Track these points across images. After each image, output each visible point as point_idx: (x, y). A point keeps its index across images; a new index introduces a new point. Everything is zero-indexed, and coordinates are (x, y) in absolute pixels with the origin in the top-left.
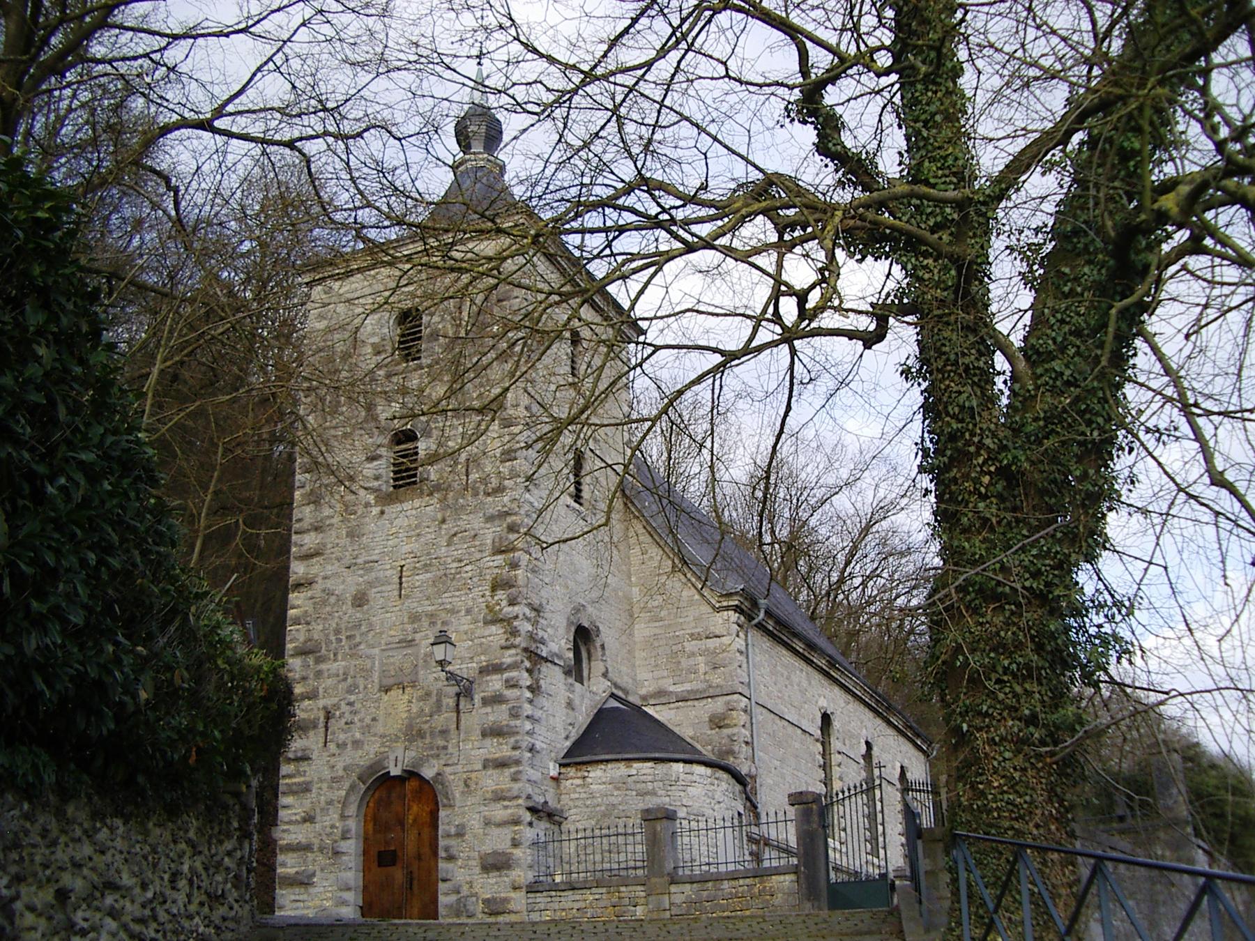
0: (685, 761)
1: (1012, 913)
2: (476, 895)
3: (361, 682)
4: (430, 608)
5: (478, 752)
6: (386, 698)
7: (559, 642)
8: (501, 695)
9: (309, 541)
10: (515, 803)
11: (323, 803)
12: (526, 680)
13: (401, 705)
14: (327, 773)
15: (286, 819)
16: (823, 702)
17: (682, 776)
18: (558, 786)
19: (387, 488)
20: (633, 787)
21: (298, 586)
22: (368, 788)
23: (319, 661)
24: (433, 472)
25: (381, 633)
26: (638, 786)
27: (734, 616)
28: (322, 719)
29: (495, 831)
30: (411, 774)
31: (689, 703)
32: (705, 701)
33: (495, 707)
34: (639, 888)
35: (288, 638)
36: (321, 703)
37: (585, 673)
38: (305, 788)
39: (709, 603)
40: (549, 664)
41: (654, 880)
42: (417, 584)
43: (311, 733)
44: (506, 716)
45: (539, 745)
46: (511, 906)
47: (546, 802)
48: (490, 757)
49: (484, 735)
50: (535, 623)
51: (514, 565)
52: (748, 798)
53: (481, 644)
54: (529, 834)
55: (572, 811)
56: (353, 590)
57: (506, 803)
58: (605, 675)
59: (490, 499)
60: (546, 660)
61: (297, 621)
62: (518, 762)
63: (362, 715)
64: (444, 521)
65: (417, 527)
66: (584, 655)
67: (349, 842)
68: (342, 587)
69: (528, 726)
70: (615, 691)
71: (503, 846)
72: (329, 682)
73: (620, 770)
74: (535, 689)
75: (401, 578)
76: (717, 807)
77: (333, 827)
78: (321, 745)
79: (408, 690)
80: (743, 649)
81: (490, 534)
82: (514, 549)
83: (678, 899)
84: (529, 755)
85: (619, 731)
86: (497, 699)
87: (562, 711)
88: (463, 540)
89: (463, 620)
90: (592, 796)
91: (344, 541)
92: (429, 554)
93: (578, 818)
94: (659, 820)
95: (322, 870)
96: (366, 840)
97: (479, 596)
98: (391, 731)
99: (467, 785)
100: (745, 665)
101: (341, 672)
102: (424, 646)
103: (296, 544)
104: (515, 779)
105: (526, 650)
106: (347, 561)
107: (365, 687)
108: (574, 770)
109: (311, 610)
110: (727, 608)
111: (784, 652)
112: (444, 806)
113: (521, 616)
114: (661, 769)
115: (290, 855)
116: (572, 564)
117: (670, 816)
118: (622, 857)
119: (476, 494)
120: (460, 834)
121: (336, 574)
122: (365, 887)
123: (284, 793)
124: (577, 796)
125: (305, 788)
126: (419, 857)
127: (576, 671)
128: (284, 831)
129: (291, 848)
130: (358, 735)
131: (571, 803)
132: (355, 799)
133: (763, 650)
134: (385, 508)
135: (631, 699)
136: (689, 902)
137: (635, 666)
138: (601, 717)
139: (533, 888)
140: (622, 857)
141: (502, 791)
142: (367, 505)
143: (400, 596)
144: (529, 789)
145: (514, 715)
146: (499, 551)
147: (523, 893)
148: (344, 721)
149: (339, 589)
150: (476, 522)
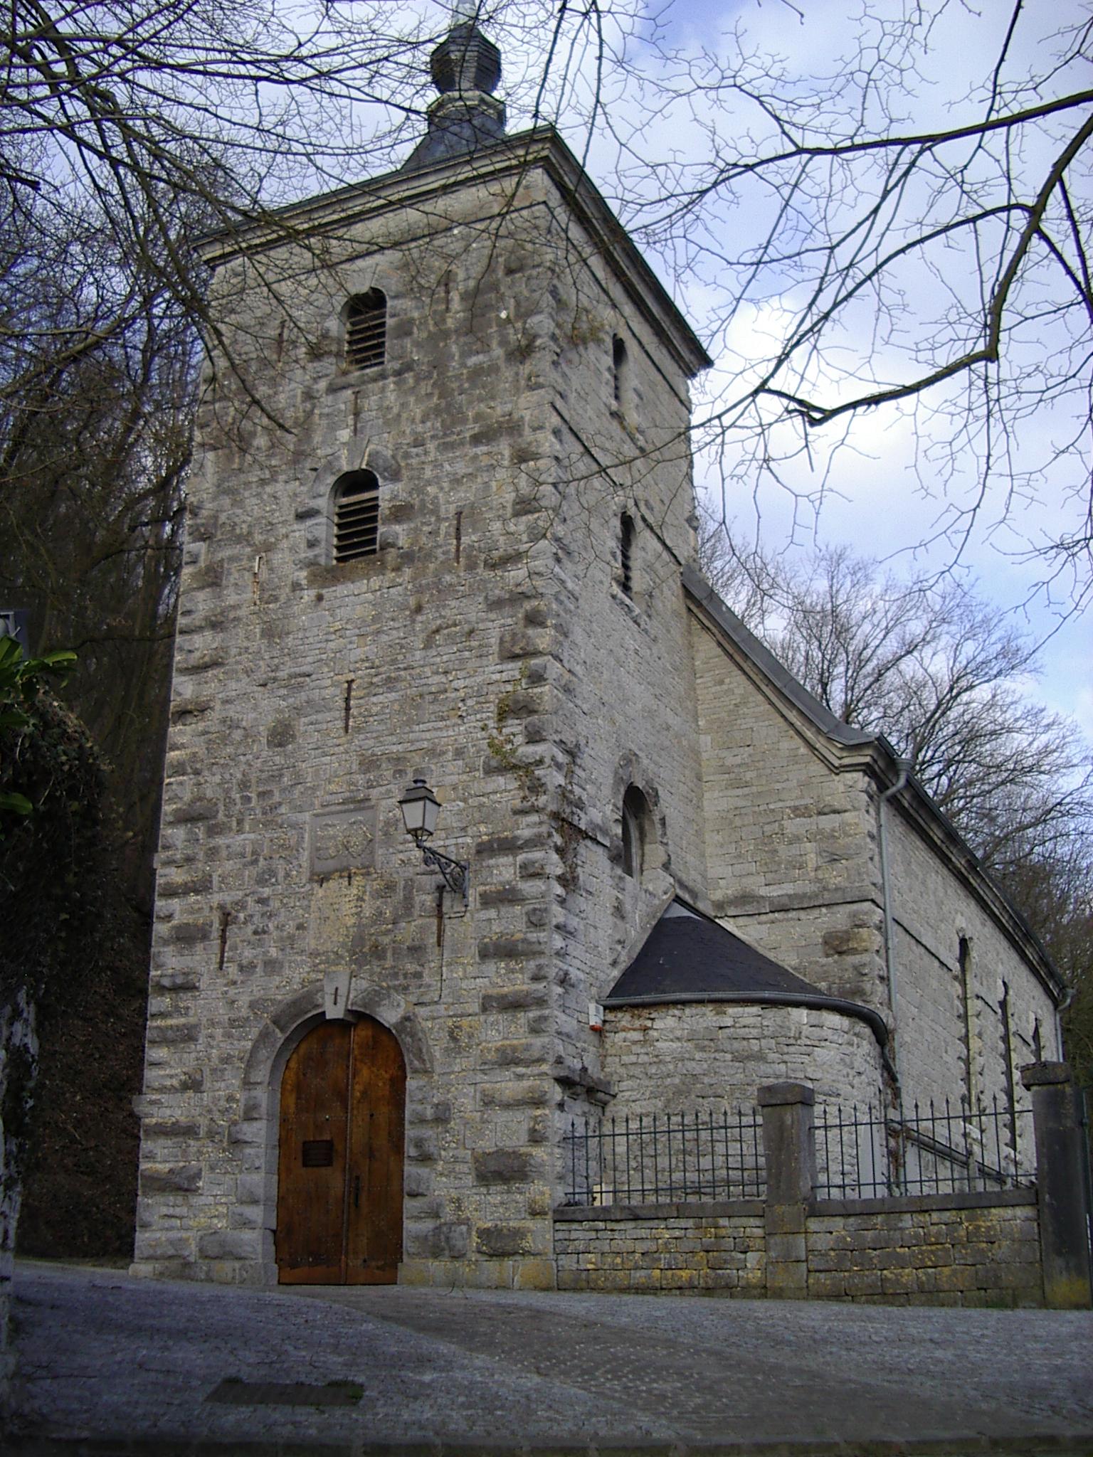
2: (467, 1222)
3: (281, 867)
4: (394, 749)
5: (470, 984)
6: (320, 892)
7: (602, 810)
8: (513, 890)
10: (535, 1070)
11: (215, 1061)
12: (555, 866)
13: (344, 906)
14: (223, 1013)
15: (156, 1085)
16: (961, 922)
17: (806, 1030)
18: (602, 1043)
19: (327, 553)
20: (727, 1046)
21: (183, 714)
22: (287, 1039)
23: (212, 831)
25: (314, 789)
26: (736, 1045)
27: (861, 780)
28: (216, 925)
29: (500, 1117)
30: (360, 1018)
31: (792, 915)
32: (816, 912)
33: (503, 910)
34: (752, 1221)
35: (165, 797)
36: (216, 899)
38: (188, 1035)
39: (824, 760)
40: (589, 843)
41: (780, 1209)
42: (375, 710)
43: (199, 947)
44: (521, 925)
45: (574, 974)
47: (584, 1069)
48: (493, 991)
49: (484, 954)
50: (570, 774)
51: (536, 678)
53: (482, 805)
54: (558, 1122)
55: (624, 1085)
56: (270, 720)
57: (521, 1070)
58: (666, 866)
60: (586, 836)
61: (180, 769)
62: (541, 1002)
63: (282, 919)
64: (419, 609)
65: (375, 619)
67: (256, 1125)
69: (558, 942)
71: (515, 1142)
72: (229, 865)
73: (705, 1018)
74: (569, 881)
75: (347, 700)
76: (856, 1081)
77: (230, 1099)
78: (214, 966)
79: (357, 880)
80: (875, 831)
81: (495, 627)
82: (536, 653)
83: (822, 1242)
84: (560, 990)
85: (684, 959)
86: (507, 897)
87: (604, 924)
88: (451, 639)
89: (450, 767)
90: (658, 1060)
91: (258, 643)
92: (394, 661)
93: (635, 1095)
94: (787, 1104)
95: (212, 1169)
96: (284, 1121)
97: (472, 732)
98: (329, 946)
99: (454, 1039)
100: (876, 858)
101: (249, 849)
103: (181, 649)
104: (535, 1030)
105: (556, 816)
106: (260, 676)
107: (287, 875)
108: (628, 1016)
111: (919, 843)
112: (415, 1071)
113: (547, 761)
114: (773, 1017)
115: (162, 1141)
116: (620, 687)
117: (805, 1099)
118: (705, 1163)
119: (471, 567)
120: (442, 1118)
122: (281, 1199)
123: (153, 1042)
124: (633, 1059)
125: (188, 1035)
126: (371, 1153)
127: (622, 858)
128: (152, 1103)
129: (163, 1131)
130: (273, 952)
131: (622, 1071)
132: (266, 1056)
134: (324, 591)
135: (701, 906)
137: (709, 857)
138: (663, 930)
139: (565, 1214)
140: (705, 1163)
141: (514, 1049)
142: (296, 586)
143: (346, 728)
144: (560, 1048)
147: (548, 1222)
148: (250, 928)
149: (248, 719)
150: (473, 611)
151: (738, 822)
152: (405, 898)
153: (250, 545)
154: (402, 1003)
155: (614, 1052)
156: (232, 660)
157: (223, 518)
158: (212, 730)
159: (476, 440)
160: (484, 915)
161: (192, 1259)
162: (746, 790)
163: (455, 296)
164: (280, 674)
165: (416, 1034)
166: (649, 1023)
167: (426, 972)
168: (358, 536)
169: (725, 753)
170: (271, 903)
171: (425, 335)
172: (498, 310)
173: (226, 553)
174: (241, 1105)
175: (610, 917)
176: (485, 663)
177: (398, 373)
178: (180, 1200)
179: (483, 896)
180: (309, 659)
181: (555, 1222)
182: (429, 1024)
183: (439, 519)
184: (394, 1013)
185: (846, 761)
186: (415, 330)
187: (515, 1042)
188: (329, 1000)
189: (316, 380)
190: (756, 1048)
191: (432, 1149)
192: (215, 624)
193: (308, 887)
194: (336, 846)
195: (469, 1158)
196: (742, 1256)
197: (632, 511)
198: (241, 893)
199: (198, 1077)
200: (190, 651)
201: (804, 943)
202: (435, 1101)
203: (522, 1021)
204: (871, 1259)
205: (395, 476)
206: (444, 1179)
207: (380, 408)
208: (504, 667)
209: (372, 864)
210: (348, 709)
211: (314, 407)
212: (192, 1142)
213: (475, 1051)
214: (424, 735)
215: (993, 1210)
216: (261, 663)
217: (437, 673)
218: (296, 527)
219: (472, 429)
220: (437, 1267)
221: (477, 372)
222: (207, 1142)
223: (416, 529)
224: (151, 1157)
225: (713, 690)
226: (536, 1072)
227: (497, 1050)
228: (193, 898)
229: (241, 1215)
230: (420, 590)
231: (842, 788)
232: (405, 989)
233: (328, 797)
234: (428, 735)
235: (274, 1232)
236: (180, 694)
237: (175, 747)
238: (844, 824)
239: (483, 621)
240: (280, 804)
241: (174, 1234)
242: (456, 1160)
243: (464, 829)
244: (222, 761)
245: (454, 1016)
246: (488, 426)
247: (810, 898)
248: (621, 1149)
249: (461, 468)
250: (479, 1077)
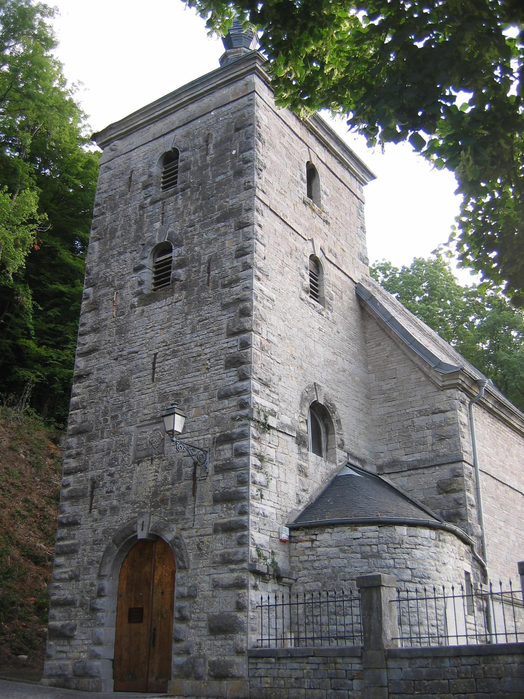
1: (113, 176)
2: (204, 657)
3: (120, 455)
4: (175, 388)
5: (209, 517)
6: (138, 469)
9: (89, 340)
13: (149, 475)
15: (58, 577)
17: (406, 539)
19: (148, 288)
21: (80, 377)
23: (89, 439)
24: (181, 273)
25: (137, 412)
28: (89, 489)
29: (222, 593)
30: (155, 538)
31: (420, 471)
36: (90, 474)
37: (324, 446)
39: (434, 383)
42: (167, 368)
44: (234, 482)
46: (235, 671)
48: (219, 521)
52: (475, 559)
53: (216, 416)
57: (233, 567)
59: (227, 290)
65: (169, 320)
67: (104, 599)
68: (111, 375)
70: (351, 461)
71: (229, 609)
72: (97, 456)
75: (154, 364)
77: (92, 585)
79: (156, 461)
81: (226, 320)
83: (396, 675)
92: (177, 341)
93: (307, 579)
96: (120, 596)
98: (141, 498)
99: (200, 549)
101: (106, 447)
106: (115, 355)
107: (123, 460)
109: (86, 396)
111: (504, 427)
112: (180, 568)
119: (215, 287)
120: (191, 596)
121: (107, 366)
124: (306, 558)
129: (58, 604)
130: (115, 503)
131: (300, 565)
135: (368, 468)
141: (229, 554)
142: (133, 306)
143: (153, 379)
146: (232, 334)
148: (105, 490)
150: (215, 310)
151: (389, 420)
152: (178, 470)
153: (112, 287)
154: (175, 530)
155: (295, 554)
156: (102, 347)
157: (101, 274)
158: (92, 384)
159: (218, 220)
160: (216, 478)
161: (70, 677)
162: (393, 403)
163: (211, 146)
164: (124, 353)
165: (181, 546)
166: (314, 537)
167: (187, 510)
168: (163, 277)
169: (382, 383)
170: (115, 476)
171: (196, 168)
172: (231, 151)
173: (103, 292)
174: (97, 587)
175: (298, 476)
176: (220, 338)
177: (183, 190)
178: (66, 643)
179: (216, 467)
180: (138, 344)
181: (249, 657)
182: (188, 541)
183: (200, 265)
184: (171, 535)
185: (446, 383)
186: (192, 167)
187: (230, 550)
188: (139, 528)
189: (145, 198)
190: (375, 551)
191: (188, 614)
192: (95, 330)
193: (132, 466)
194: (146, 443)
195: (206, 618)
196: (350, 682)
197: (319, 254)
198: (101, 471)
199: (77, 572)
200: (84, 344)
201: (427, 487)
202: (190, 585)
203: (234, 538)
204: (425, 687)
205: (180, 245)
206: (193, 631)
207: (174, 209)
208: (229, 340)
209: (163, 453)
210: (154, 368)
211: (144, 213)
212: (73, 609)
214: (190, 380)
215: (500, 658)
216: (115, 348)
217: (196, 346)
218: (134, 275)
219: (218, 214)
220: (188, 684)
221: (220, 185)
222: (80, 609)
223: (189, 270)
224: (53, 618)
225: (375, 349)
226: (240, 567)
227: (221, 555)
228: (79, 475)
229: (93, 651)
230: (189, 303)
231: (445, 399)
232: (176, 521)
233: (143, 417)
234: (191, 380)
235: (113, 660)
236: (78, 367)
237: (75, 395)
238: (446, 418)
239: (219, 316)
240: (121, 422)
241: (62, 662)
242: (199, 620)
243: (208, 430)
244: (96, 401)
245: (201, 535)
246: (225, 212)
247: (429, 461)
248: (301, 611)
249: (211, 236)
250: (212, 571)
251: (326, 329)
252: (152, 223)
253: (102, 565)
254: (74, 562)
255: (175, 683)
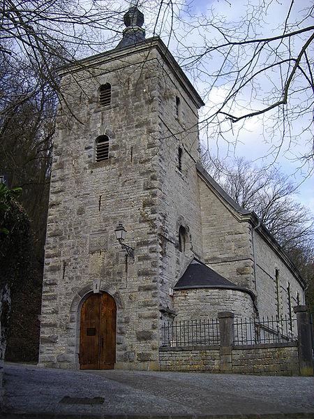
0: (233, 289)
7: (173, 233)
9: (58, 185)
13: (99, 260)
16: (276, 265)
19: (94, 159)
23: (61, 239)
24: (115, 153)
29: (144, 321)
36: (62, 259)
37: (183, 249)
38: (54, 298)
44: (150, 266)
47: (168, 307)
49: (139, 275)
54: (160, 323)
57: (149, 308)
58: (191, 249)
61: (51, 221)
62: (156, 288)
64: (120, 175)
66: (182, 240)
72: (66, 249)
73: (203, 292)
81: (142, 181)
83: (236, 357)
86: (146, 258)
89: (129, 221)
91: (74, 185)
94: (226, 318)
97: (135, 211)
102: (111, 232)
105: (160, 235)
106: (75, 194)
110: (245, 221)
114: (222, 292)
117: (232, 316)
118: (203, 334)
119: (135, 163)
120: (127, 322)
122: (81, 345)
125: (54, 298)
133: (257, 239)
136: (242, 359)
137: (204, 247)
140: (203, 334)
141: (148, 302)
142: (85, 169)
145: (154, 265)
147: (157, 352)
150: (136, 176)
159: (137, 126)
163: (131, 85)
168: (103, 154)
197: (182, 147)
205: (114, 137)
213: (137, 302)
220: (126, 364)
221: (137, 107)
224: (43, 333)
228: (55, 258)
249: (132, 135)
251: (185, 187)
252: (96, 123)
253: (72, 305)
254: (54, 304)
255: (118, 364)
